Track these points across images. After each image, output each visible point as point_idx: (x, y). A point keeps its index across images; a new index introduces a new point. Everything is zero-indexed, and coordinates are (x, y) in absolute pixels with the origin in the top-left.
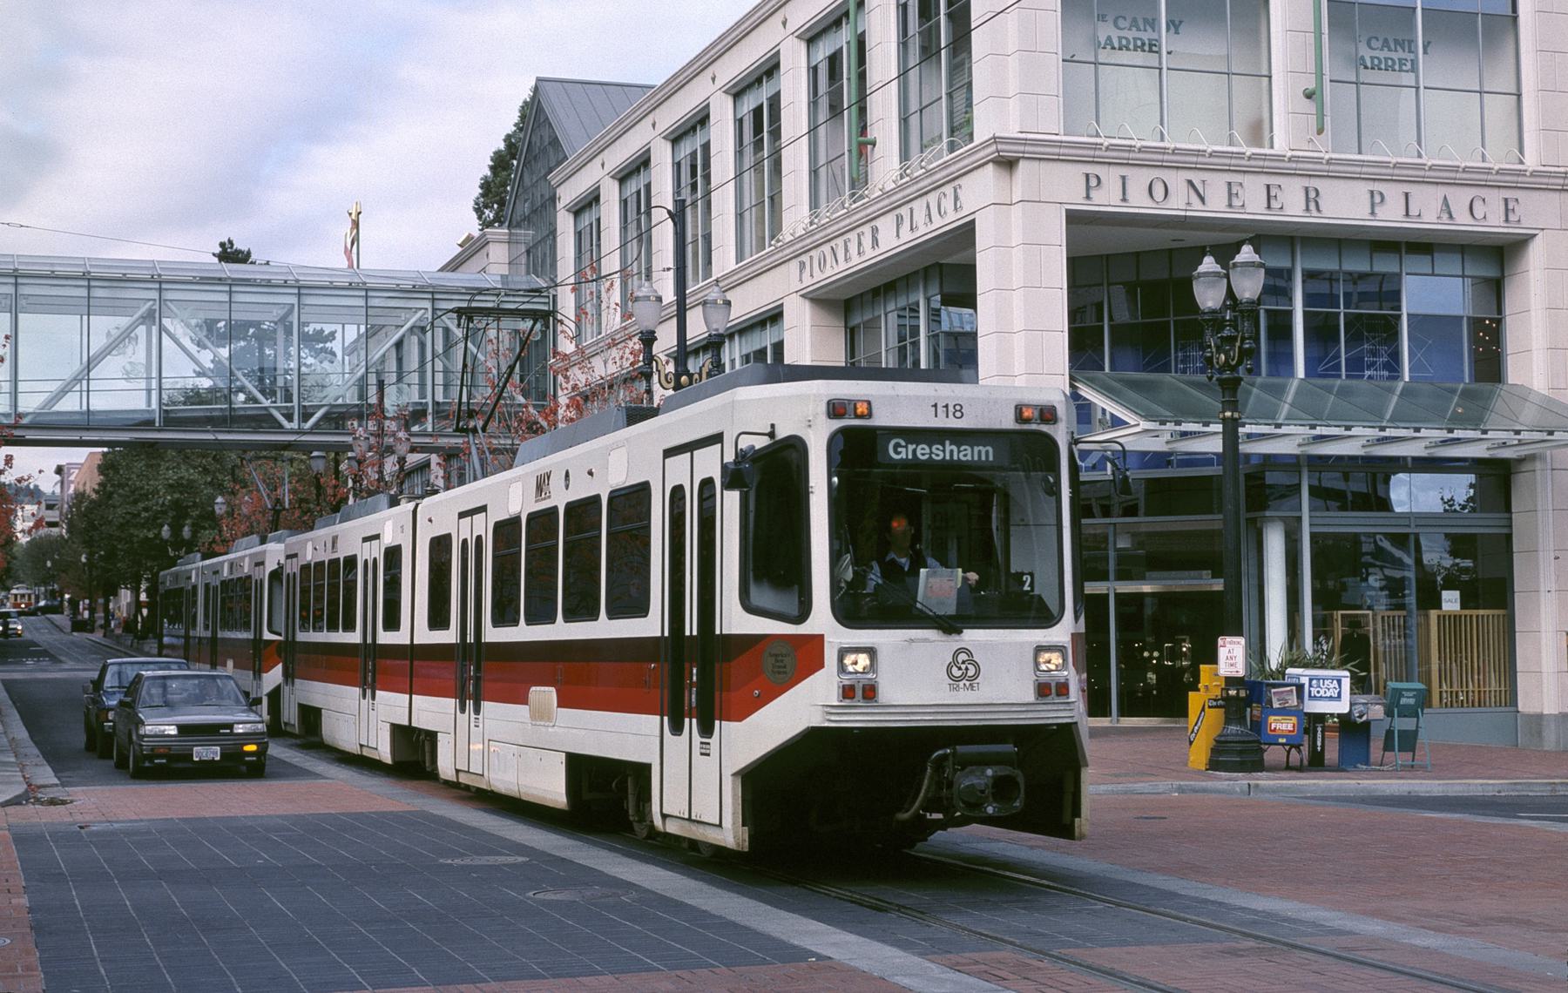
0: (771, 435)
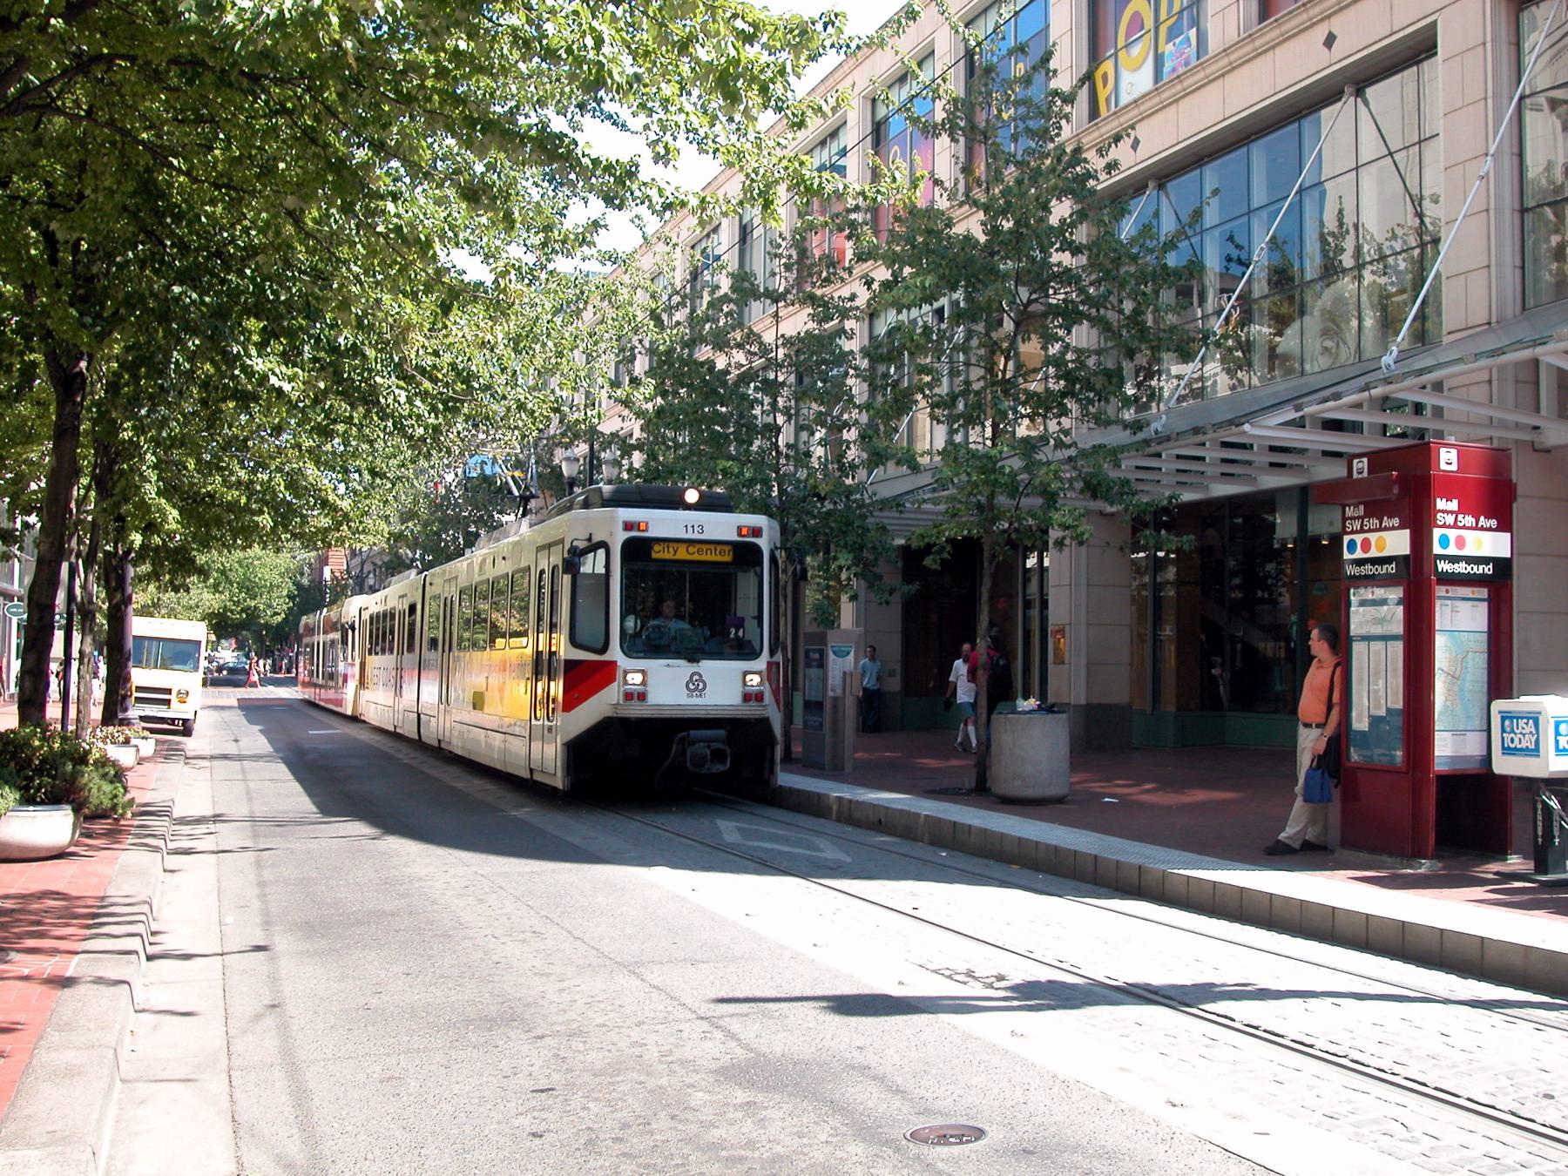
0: (590, 539)
